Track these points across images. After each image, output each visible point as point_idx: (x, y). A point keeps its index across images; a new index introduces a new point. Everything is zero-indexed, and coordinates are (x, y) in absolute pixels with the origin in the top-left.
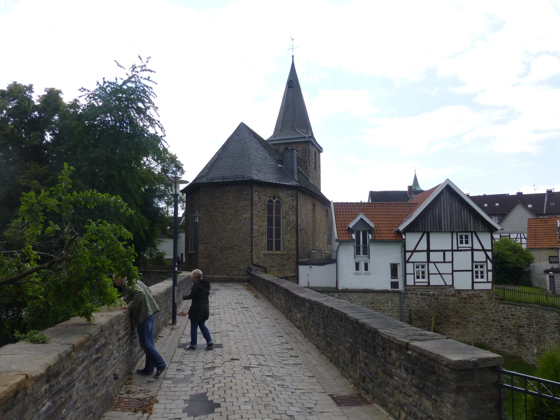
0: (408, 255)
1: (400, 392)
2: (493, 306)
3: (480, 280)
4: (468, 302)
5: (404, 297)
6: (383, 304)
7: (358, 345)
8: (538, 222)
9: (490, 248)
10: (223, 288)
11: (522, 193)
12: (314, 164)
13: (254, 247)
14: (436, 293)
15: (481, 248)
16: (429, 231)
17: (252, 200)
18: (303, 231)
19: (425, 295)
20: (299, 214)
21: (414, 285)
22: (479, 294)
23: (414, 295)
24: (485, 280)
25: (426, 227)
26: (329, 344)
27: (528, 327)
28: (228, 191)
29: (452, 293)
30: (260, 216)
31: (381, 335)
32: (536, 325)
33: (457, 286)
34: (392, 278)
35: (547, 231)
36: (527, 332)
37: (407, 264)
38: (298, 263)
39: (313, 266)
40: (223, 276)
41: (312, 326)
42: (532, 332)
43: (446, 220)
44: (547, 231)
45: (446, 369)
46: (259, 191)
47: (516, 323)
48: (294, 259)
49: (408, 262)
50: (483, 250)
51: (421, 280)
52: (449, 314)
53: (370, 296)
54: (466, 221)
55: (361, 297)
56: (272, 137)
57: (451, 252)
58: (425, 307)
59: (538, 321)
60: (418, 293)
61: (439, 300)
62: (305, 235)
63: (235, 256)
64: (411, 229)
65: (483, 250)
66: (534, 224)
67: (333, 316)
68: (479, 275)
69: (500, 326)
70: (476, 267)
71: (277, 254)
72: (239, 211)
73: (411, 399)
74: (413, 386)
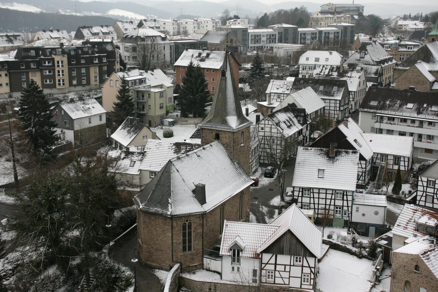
0: (263, 265)
3: (306, 283)
13: (173, 252)
15: (308, 266)
17: (172, 226)
28: (159, 217)
37: (262, 270)
49: (263, 269)
51: (270, 280)
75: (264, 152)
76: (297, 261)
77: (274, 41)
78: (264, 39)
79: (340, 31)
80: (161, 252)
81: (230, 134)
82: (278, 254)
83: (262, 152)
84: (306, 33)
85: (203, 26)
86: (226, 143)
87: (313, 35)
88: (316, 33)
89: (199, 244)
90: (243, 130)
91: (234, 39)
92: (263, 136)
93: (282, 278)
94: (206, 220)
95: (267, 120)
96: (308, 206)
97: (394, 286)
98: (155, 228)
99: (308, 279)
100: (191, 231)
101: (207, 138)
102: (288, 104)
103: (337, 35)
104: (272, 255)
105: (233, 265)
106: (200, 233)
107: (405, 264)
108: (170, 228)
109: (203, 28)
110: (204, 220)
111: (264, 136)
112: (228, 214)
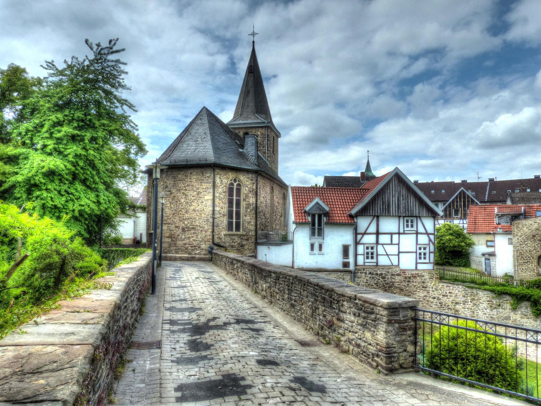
0: (359, 237)
1: (350, 332)
2: (434, 285)
3: (423, 261)
4: (411, 280)
7: (318, 302)
8: (478, 209)
9: (433, 232)
10: (186, 266)
11: (466, 181)
12: (272, 148)
13: (215, 227)
14: (383, 272)
16: (379, 215)
17: (214, 182)
18: (262, 213)
19: (373, 274)
20: (258, 197)
21: (364, 265)
23: (363, 274)
24: (427, 261)
25: (376, 211)
26: (293, 306)
27: (463, 304)
28: (191, 173)
29: (397, 273)
30: (222, 198)
31: (336, 291)
32: (471, 302)
33: (403, 266)
34: (344, 258)
35: (486, 217)
36: (462, 308)
38: (257, 244)
39: (271, 247)
40: (185, 255)
41: (277, 293)
42: (467, 308)
44: (486, 217)
45: (381, 309)
47: (454, 300)
48: (253, 240)
50: (427, 233)
54: (412, 207)
56: (232, 121)
57: (398, 235)
59: (473, 298)
60: (368, 272)
61: (386, 279)
62: (263, 217)
63: (197, 236)
64: (363, 212)
65: (427, 233)
66: (474, 211)
67: (297, 282)
68: (422, 256)
69: (440, 303)
70: (420, 249)
71: (237, 235)
72: (200, 193)
73: (357, 335)
74: (358, 325)
80: (192, 231)
97: (520, 270)
98: (184, 191)
105: (313, 241)
106: (253, 204)
107: (534, 233)
108: (211, 185)
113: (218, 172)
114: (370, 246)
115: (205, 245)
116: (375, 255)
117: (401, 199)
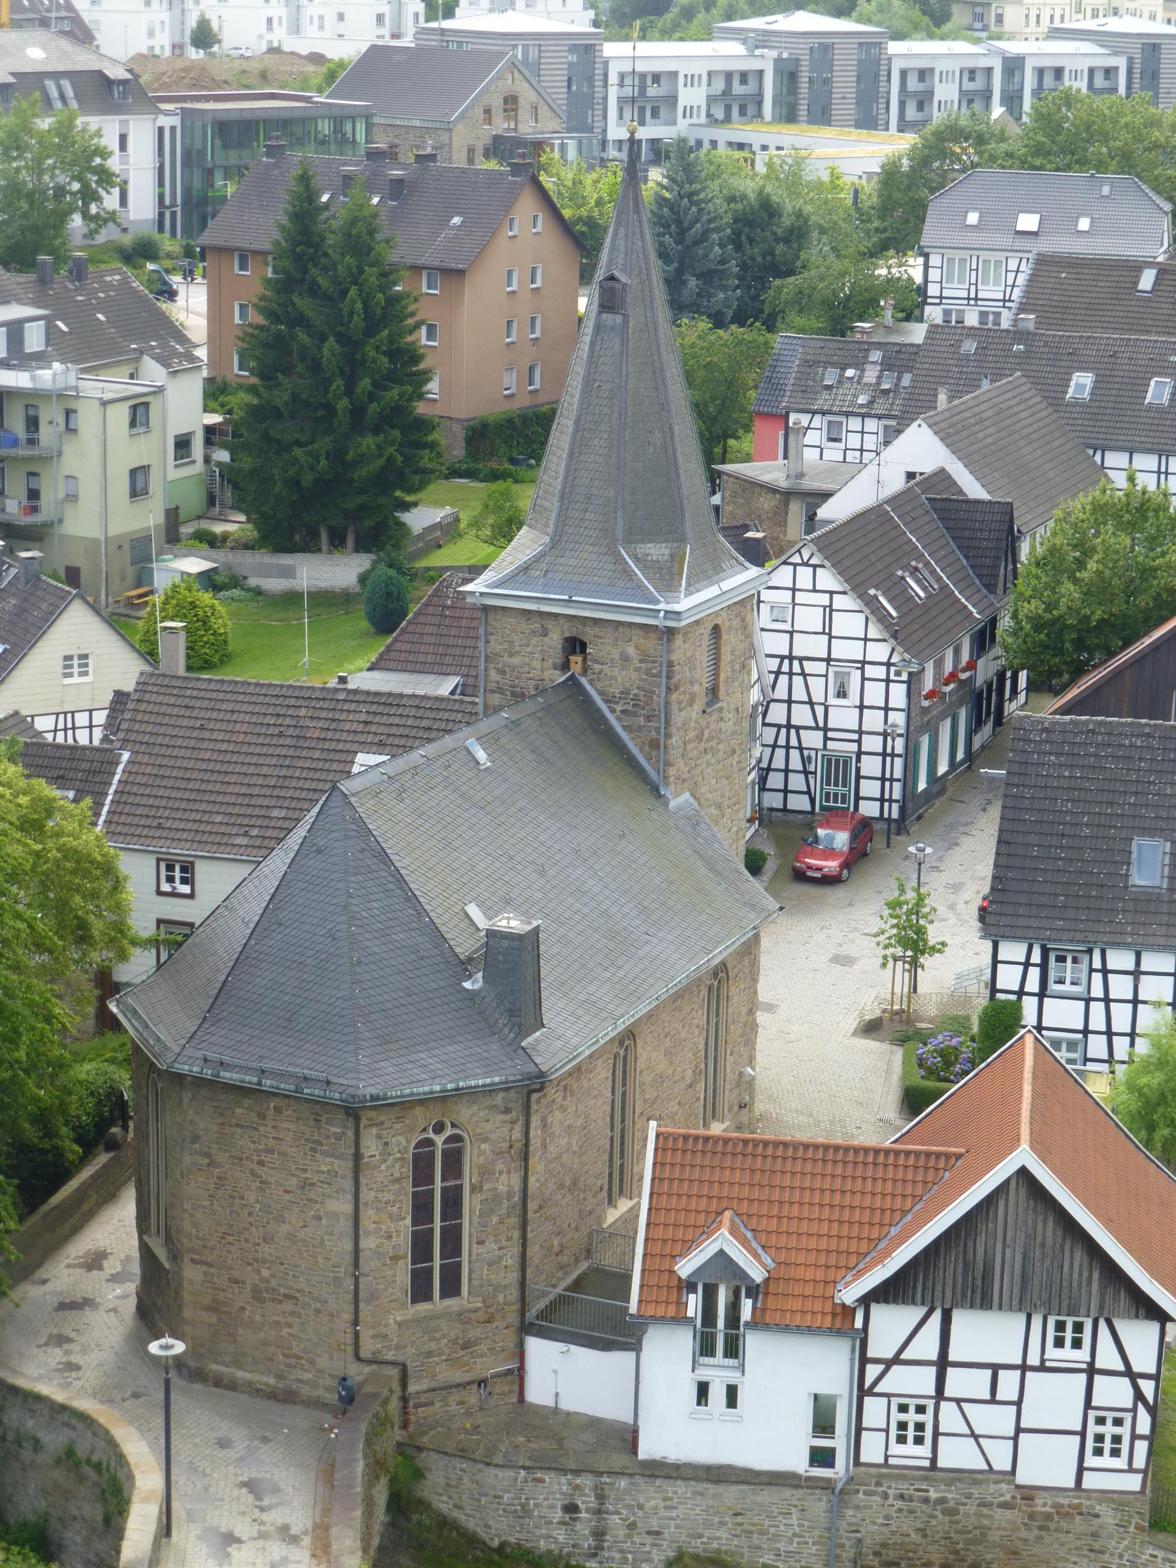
0: (872, 1371)
2: (1127, 1548)
3: (1106, 1461)
4: (1052, 1526)
5: (841, 1500)
6: (771, 1517)
13: (362, 1305)
14: (950, 1496)
15: (1121, 1368)
17: (357, 1157)
19: (911, 1500)
22: (1092, 1507)
23: (877, 1498)
28: (278, 1110)
29: (1002, 1499)
30: (387, 1203)
33: (1024, 1477)
37: (867, 1400)
40: (265, 1379)
43: (1006, 1278)
46: (382, 1123)
48: (513, 1318)
49: (870, 1392)
50: (1129, 1373)
51: (910, 1449)
52: (989, 1557)
53: (730, 1494)
54: (1075, 1284)
55: (702, 1495)
58: (908, 1535)
60: (891, 1492)
64: (891, 1292)
65: (1129, 1373)
68: (1107, 1445)
72: (313, 1185)
75: (788, 747)
76: (1059, 1343)
77: (750, 107)
78: (692, 97)
79: (1121, 63)
80: (288, 1306)
81: (651, 644)
82: (955, 1304)
83: (774, 746)
84: (932, 70)
85: (321, 18)
86: (625, 692)
87: (972, 79)
88: (989, 70)
89: (500, 1258)
90: (719, 621)
91: (527, 96)
92: (782, 658)
93: (975, 1437)
94: (544, 1124)
95: (806, 564)
96: (1072, 1046)
98: (257, 1168)
99: (1117, 1439)
100: (459, 1189)
101: (515, 660)
102: (911, 476)
103: (920, 87)
104: (921, 1311)
106: (510, 1194)
108: (346, 1166)
109: (321, 27)
110: (533, 1125)
111: (791, 658)
112: (650, 1094)
113: (371, 1119)
114: (912, 1403)
115: (331, 1358)
116: (928, 1434)
117: (1038, 1254)
